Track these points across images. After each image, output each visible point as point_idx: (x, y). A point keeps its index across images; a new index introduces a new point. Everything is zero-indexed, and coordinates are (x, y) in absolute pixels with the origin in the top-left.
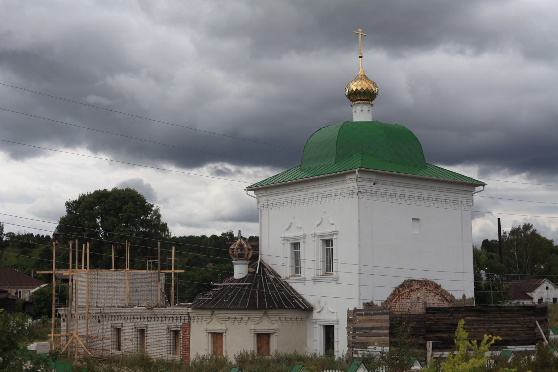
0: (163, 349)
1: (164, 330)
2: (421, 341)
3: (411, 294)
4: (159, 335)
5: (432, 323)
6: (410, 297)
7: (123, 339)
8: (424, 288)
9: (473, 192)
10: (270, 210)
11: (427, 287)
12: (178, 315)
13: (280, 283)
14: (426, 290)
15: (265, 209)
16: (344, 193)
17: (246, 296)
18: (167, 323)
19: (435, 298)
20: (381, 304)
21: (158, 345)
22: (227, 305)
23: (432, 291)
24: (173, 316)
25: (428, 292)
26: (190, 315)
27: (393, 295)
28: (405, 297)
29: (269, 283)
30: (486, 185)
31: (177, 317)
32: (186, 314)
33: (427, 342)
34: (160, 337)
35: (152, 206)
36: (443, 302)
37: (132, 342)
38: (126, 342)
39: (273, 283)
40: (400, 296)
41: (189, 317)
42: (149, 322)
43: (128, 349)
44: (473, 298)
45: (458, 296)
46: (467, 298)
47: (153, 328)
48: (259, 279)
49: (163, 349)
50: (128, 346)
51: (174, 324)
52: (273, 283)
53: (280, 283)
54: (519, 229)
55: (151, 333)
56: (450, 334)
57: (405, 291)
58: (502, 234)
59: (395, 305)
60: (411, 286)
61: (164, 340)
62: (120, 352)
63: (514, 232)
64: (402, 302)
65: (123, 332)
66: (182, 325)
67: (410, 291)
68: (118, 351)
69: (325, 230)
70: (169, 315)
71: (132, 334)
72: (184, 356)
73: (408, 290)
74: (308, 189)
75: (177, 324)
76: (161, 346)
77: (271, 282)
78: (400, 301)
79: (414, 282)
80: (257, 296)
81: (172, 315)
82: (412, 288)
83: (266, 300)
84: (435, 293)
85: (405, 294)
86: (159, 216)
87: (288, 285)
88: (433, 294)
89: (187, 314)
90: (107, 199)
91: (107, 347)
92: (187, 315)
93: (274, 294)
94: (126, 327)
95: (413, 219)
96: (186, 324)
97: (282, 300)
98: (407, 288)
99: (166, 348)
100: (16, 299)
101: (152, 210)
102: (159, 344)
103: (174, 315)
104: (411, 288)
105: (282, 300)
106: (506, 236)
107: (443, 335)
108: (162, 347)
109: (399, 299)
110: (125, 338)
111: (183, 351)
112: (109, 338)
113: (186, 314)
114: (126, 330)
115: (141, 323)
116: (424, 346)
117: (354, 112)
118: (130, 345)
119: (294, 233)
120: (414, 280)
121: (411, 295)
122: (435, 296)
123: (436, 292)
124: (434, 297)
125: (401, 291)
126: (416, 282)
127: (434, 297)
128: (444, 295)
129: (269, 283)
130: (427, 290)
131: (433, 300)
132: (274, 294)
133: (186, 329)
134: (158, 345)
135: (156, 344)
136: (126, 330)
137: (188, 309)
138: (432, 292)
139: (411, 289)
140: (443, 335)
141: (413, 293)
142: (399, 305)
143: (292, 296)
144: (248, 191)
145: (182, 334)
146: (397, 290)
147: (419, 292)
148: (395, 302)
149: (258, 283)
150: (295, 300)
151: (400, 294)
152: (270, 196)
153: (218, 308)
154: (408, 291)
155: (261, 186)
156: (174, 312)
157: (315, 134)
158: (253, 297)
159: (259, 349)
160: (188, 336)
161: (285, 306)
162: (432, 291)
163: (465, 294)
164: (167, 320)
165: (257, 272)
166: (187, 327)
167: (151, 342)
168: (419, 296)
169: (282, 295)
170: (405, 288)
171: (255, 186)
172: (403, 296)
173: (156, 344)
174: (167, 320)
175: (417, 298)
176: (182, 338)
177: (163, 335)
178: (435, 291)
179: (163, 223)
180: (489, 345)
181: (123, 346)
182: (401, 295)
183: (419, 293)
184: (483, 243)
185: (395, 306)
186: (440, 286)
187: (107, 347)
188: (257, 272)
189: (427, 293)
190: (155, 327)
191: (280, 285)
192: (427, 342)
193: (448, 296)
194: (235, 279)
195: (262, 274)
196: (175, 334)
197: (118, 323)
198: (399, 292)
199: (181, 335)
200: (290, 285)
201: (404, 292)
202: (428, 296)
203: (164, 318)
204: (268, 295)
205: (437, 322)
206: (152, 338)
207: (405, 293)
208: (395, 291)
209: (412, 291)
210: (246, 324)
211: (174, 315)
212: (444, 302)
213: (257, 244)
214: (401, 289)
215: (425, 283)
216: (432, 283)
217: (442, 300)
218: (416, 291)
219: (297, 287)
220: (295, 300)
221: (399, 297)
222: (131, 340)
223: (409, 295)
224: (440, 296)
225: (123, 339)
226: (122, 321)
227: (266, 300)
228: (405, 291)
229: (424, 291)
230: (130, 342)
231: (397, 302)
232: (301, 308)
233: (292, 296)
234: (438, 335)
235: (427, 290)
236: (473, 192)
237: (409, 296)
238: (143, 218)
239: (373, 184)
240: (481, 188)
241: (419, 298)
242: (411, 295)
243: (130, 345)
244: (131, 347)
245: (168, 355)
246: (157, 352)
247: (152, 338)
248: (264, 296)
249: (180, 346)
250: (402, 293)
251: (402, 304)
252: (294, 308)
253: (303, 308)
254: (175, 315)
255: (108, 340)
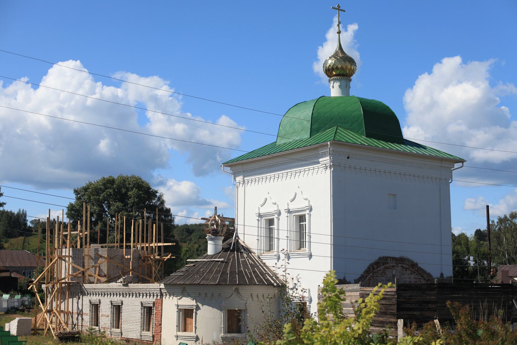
0: (137, 325)
1: (138, 306)
2: (393, 320)
3: (386, 271)
4: (133, 311)
5: (404, 300)
6: (385, 274)
7: (100, 314)
8: (400, 265)
9: (452, 169)
10: (246, 185)
11: (403, 265)
12: (150, 291)
13: (254, 259)
14: (402, 267)
15: (241, 185)
16: (317, 167)
17: (217, 272)
18: (140, 299)
19: (412, 276)
20: (354, 281)
21: (132, 321)
22: (198, 280)
23: (409, 268)
24: (146, 292)
25: (404, 269)
26: (162, 291)
27: (367, 272)
28: (380, 274)
29: (242, 260)
30: (466, 161)
31: (150, 293)
32: (158, 289)
33: (398, 320)
34: (135, 313)
35: (156, 192)
36: (420, 280)
37: (108, 318)
38: (103, 318)
39: (246, 259)
40: (375, 274)
41: (162, 295)
42: (124, 298)
43: (105, 325)
44: (451, 277)
45: (436, 274)
46: (445, 276)
47: (128, 304)
48: (233, 255)
49: (137, 325)
50: (105, 322)
51: (147, 300)
52: (246, 259)
53: (254, 259)
54: (506, 217)
55: (126, 309)
56: (423, 312)
57: (380, 268)
58: (490, 223)
59: (369, 282)
60: (386, 263)
61: (138, 316)
62: (98, 327)
63: (501, 221)
64: (376, 280)
65: (100, 307)
66: (154, 301)
67: (385, 268)
68: (116, 329)
69: (299, 205)
70: (143, 291)
71: (109, 309)
72: (156, 332)
73: (383, 267)
74: (282, 164)
75: (149, 301)
76: (135, 322)
77: (245, 258)
78: (375, 279)
79: (389, 259)
80: (229, 272)
81: (145, 291)
82: (387, 265)
83: (237, 276)
84: (411, 270)
85: (379, 272)
86: (163, 203)
87: (262, 262)
88: (410, 272)
89: (159, 289)
90: (112, 185)
91: (86, 323)
92: (159, 291)
93: (247, 271)
94: (104, 303)
95: (389, 194)
96: (159, 300)
97: (254, 276)
98: (381, 265)
99: (139, 324)
100: (18, 278)
101: (156, 196)
102: (133, 320)
103: (147, 291)
104: (386, 265)
105: (254, 276)
106: (495, 225)
107: (415, 313)
108: (136, 323)
109: (374, 276)
110: (102, 313)
111: (155, 327)
112: (88, 314)
113: (158, 289)
114: (103, 306)
115: (117, 299)
116: (396, 323)
117: (331, 88)
118: (107, 321)
119: (269, 209)
120: (390, 257)
121: (386, 272)
122: (411, 274)
123: (413, 270)
124: (410, 275)
125: (375, 268)
126: (392, 259)
127: (410, 275)
128: (421, 272)
129: (242, 260)
130: (404, 268)
131: (410, 278)
132: (247, 271)
133: (159, 305)
134: (132, 321)
135: (130, 320)
136: (103, 306)
137: (160, 285)
138: (408, 270)
139: (386, 266)
140: (415, 313)
141: (388, 270)
142: (373, 282)
143: (265, 272)
144: (225, 168)
145: (154, 311)
146: (371, 267)
147: (395, 269)
148: (369, 280)
149: (231, 259)
150: (268, 277)
151: (375, 271)
152: (246, 172)
153: (188, 283)
154: (383, 269)
155: (237, 161)
156: (147, 288)
157: (291, 109)
158: (224, 273)
159: (229, 326)
160: (160, 313)
161: (257, 283)
162: (409, 268)
163: (443, 273)
164: (141, 296)
165: (231, 248)
166: (159, 304)
167: (126, 318)
168: (394, 274)
169: (254, 272)
170: (380, 265)
171: (231, 162)
172: (377, 273)
173: (130, 320)
174: (141, 296)
175: (392, 276)
176: (154, 314)
177: (137, 311)
178: (411, 269)
179: (167, 208)
180: (88, 244)
181: (100, 322)
182: (375, 272)
183: (394, 271)
184: (475, 232)
185: (369, 284)
186: (417, 264)
187: (86, 323)
188: (231, 248)
189: (403, 270)
190: (129, 303)
191: (253, 261)
192: (398, 320)
193: (425, 274)
194: (208, 255)
195: (236, 249)
196: (148, 310)
197: (96, 299)
198: (374, 269)
199: (154, 311)
200: (264, 261)
201: (378, 269)
202: (404, 274)
203: (138, 294)
204: (240, 272)
205: (409, 299)
206: (127, 314)
207: (380, 270)
208: (369, 268)
209: (387, 268)
210: (216, 300)
211: (147, 291)
212: (421, 280)
213: (233, 221)
214: (375, 266)
215: (401, 260)
216: (408, 260)
217: (419, 278)
218: (391, 268)
219: (270, 263)
220: (268, 277)
221: (373, 274)
222: (108, 316)
223: (384, 272)
224: (417, 274)
225: (100, 315)
226: (100, 297)
227: (237, 276)
228: (380, 268)
229: (399, 269)
230: (107, 318)
231: (371, 280)
232: (273, 285)
233: (265, 272)
234: (410, 313)
235: (404, 268)
236: (452, 169)
237: (383, 273)
238: (148, 203)
239: (347, 158)
240: (461, 164)
241: (394, 275)
242: (386, 272)
243: (107, 321)
244: (107, 322)
245: (141, 332)
246: (131, 328)
247: (127, 314)
248: (236, 272)
249: (153, 321)
250: (377, 270)
251: (376, 281)
252: (266, 285)
253: (275, 284)
254: (148, 291)
255: (87, 316)
